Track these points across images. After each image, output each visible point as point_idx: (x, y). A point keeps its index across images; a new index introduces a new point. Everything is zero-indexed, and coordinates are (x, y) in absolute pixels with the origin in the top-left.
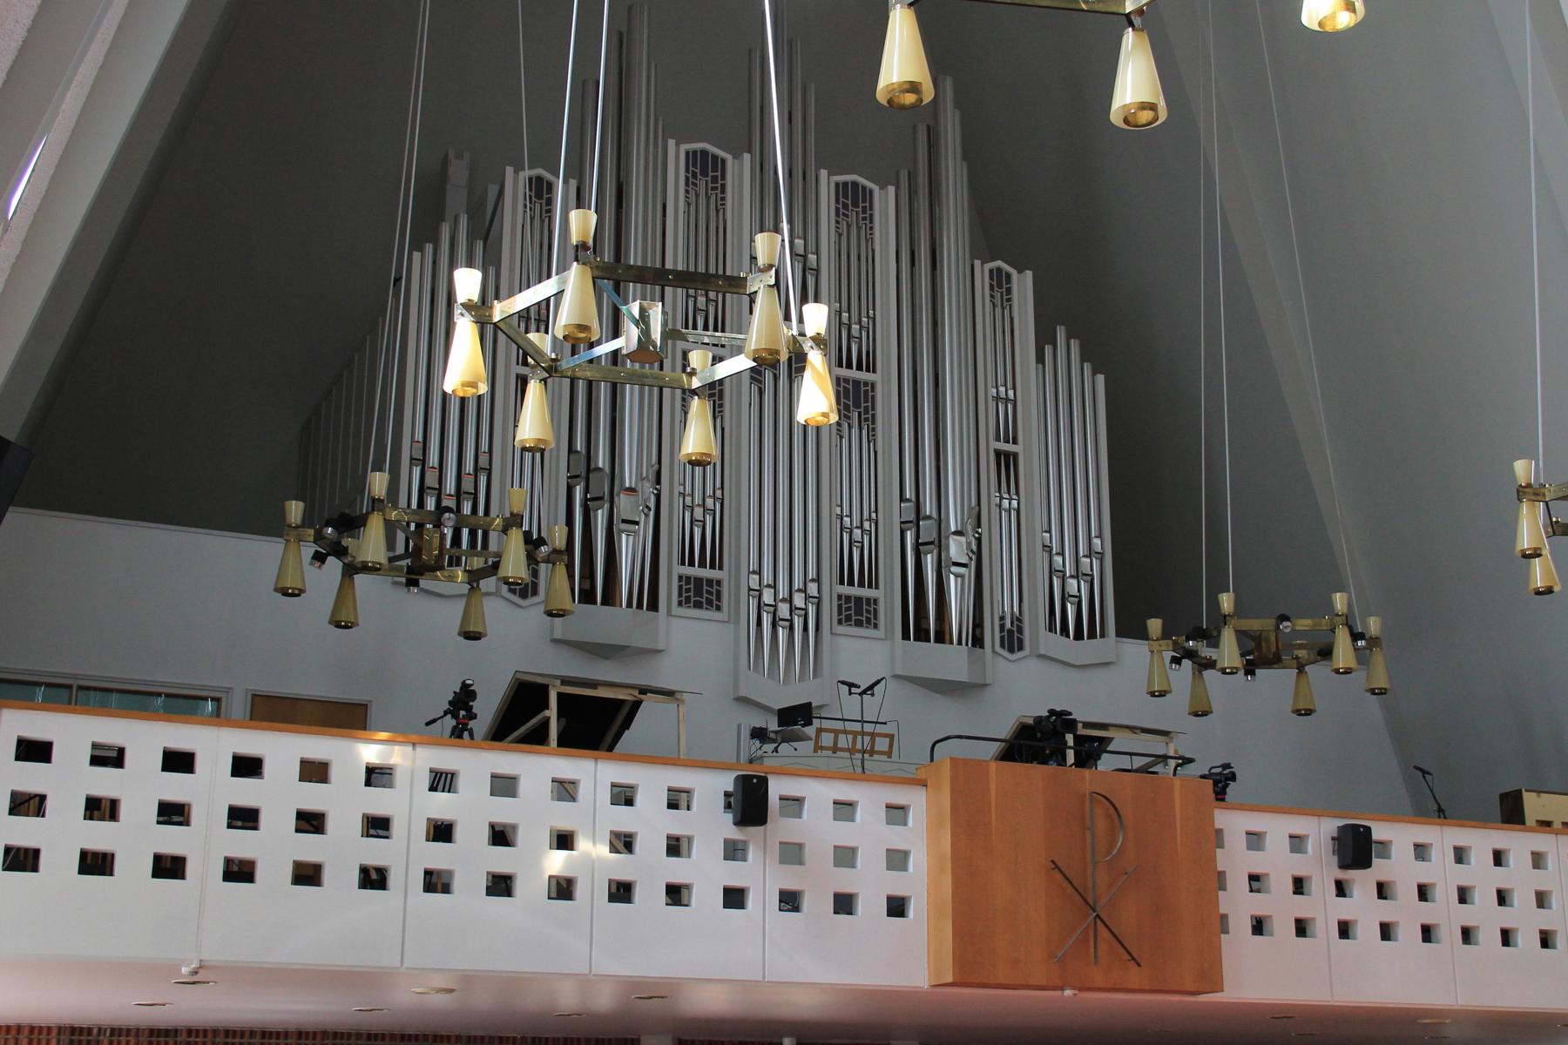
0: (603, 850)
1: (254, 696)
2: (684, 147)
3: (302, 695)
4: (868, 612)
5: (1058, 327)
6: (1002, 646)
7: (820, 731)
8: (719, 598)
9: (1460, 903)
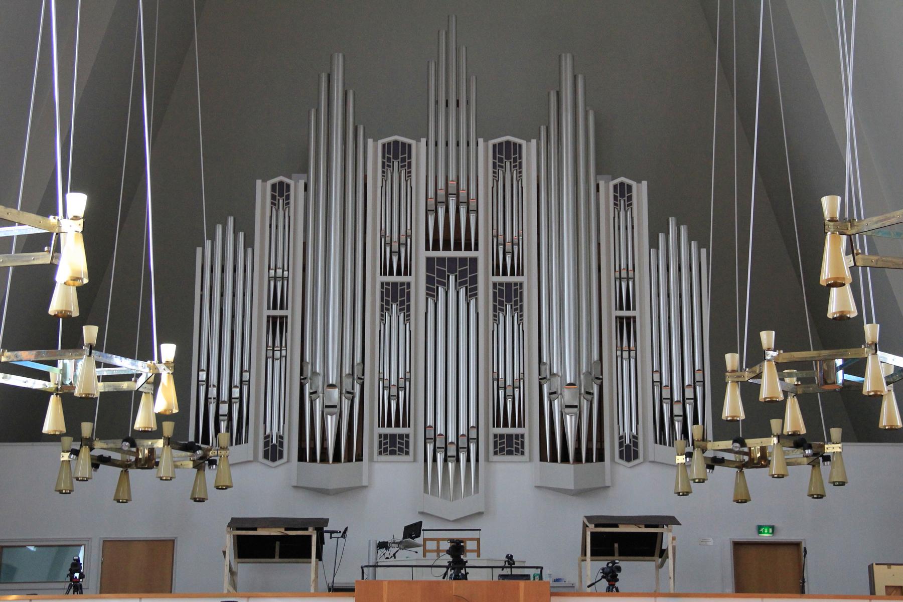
3: (138, 538)
4: (517, 444)
5: (670, 218)
6: (621, 457)
7: (425, 540)
8: (407, 446)
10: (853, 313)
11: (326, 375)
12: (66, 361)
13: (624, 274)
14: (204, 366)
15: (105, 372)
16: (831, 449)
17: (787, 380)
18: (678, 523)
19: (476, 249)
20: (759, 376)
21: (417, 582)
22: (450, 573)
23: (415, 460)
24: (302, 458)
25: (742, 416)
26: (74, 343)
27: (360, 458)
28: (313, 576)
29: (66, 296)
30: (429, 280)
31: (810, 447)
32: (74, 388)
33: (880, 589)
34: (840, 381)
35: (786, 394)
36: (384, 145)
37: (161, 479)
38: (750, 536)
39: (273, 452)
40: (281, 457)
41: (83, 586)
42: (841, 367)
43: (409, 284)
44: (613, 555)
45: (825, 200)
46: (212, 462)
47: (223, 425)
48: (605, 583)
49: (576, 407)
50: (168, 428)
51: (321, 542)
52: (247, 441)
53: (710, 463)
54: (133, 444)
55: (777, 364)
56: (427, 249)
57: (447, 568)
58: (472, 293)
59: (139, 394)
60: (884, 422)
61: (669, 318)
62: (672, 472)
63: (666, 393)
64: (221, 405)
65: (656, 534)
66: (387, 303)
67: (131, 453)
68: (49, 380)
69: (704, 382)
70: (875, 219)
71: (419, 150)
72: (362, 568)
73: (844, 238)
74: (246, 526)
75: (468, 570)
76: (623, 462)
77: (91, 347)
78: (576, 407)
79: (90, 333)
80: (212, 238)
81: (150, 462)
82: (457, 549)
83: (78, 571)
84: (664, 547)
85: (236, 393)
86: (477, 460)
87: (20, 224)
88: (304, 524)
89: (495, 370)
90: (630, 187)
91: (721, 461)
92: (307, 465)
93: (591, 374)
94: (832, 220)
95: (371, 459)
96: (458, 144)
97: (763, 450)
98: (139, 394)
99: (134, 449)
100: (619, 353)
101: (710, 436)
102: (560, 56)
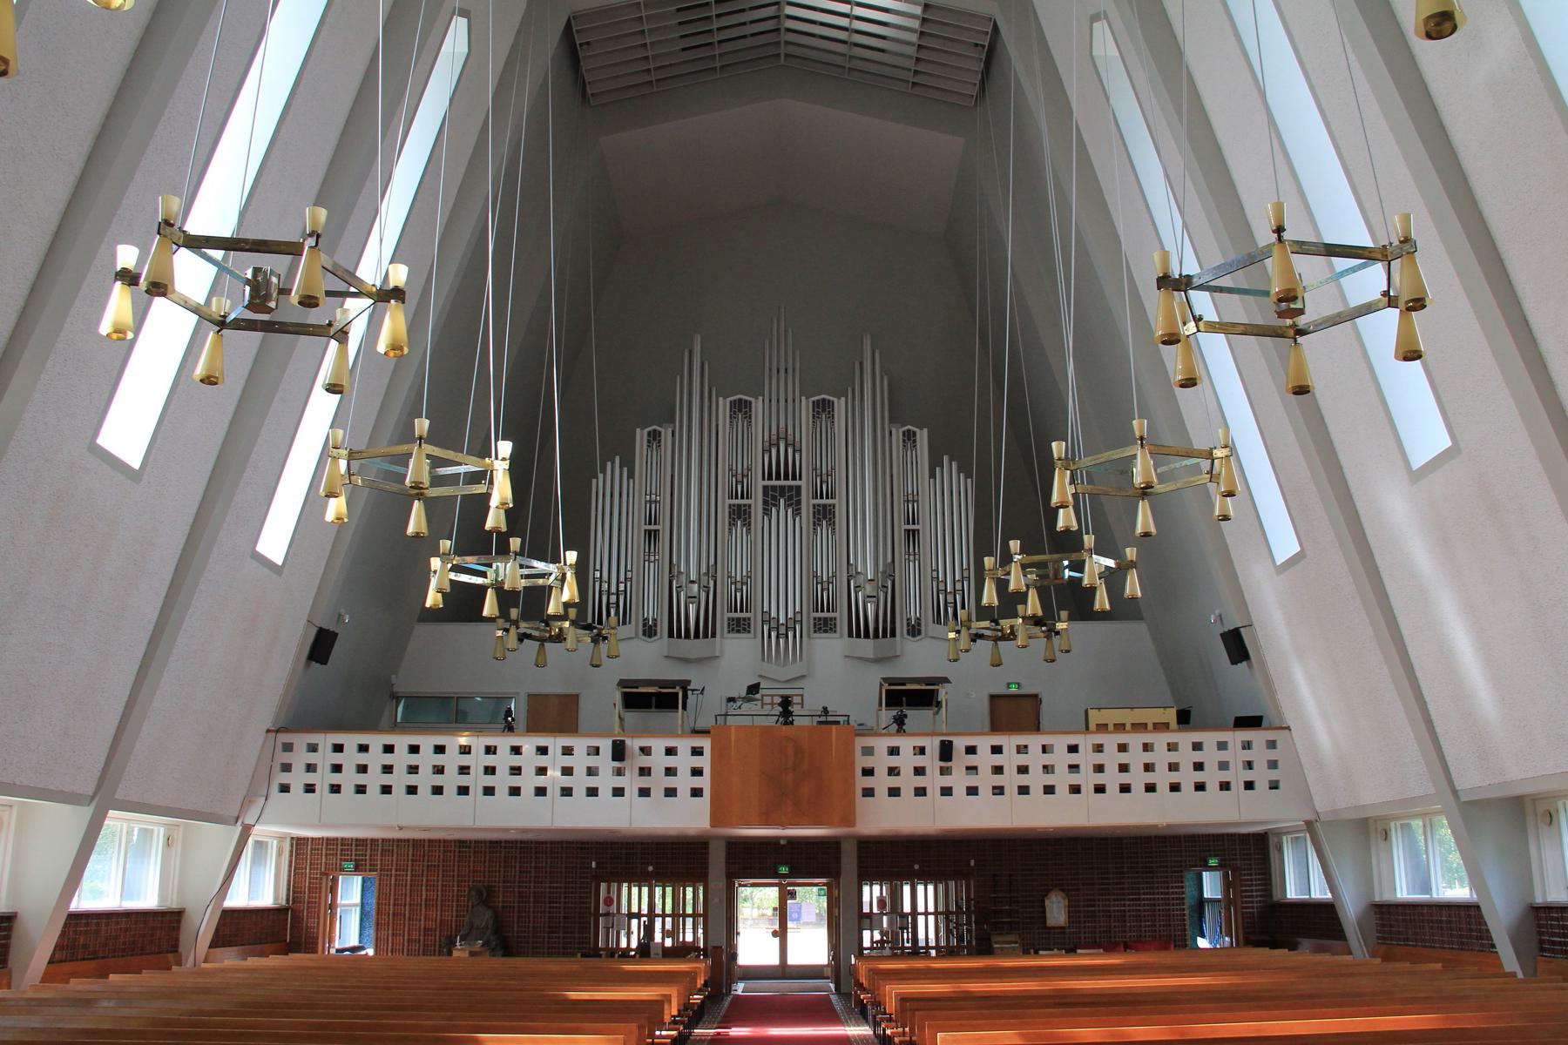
0: (559, 773)
1: (529, 695)
2: (729, 400)
6: (908, 634)
7: (763, 696)
8: (749, 626)
9: (1145, 771)
10: (1075, 526)
11: (688, 574)
12: (499, 564)
13: (910, 498)
14: (598, 567)
15: (526, 571)
16: (1060, 626)
17: (1029, 576)
18: (948, 681)
19: (800, 479)
20: (1009, 574)
21: (756, 727)
22: (781, 719)
23: (755, 637)
24: (671, 635)
25: (996, 603)
26: (504, 551)
27: (714, 635)
28: (680, 722)
29: (497, 517)
30: (765, 502)
31: (1045, 625)
32: (504, 584)
33: (1092, 727)
34: (1067, 577)
35: (1028, 587)
36: (731, 402)
37: (568, 650)
38: (1001, 690)
39: (650, 631)
40: (655, 634)
41: (515, 727)
42: (1067, 567)
43: (750, 506)
44: (902, 706)
45: (1054, 445)
46: (605, 638)
47: (613, 611)
48: (895, 727)
49: (874, 597)
50: (572, 612)
51: (685, 697)
52: (630, 623)
53: (974, 638)
54: (547, 625)
55: (1021, 565)
56: (764, 479)
57: (779, 716)
58: (797, 512)
59: (551, 588)
60: (1097, 606)
61: (944, 530)
62: (947, 644)
63: (942, 587)
64: (611, 596)
65: (933, 690)
66: (735, 413)
67: (547, 631)
68: (486, 578)
69: (969, 578)
70: (1090, 458)
71: (758, 405)
72: (716, 716)
73: (1068, 472)
74: (630, 685)
75: (794, 718)
76: (910, 638)
77: (516, 554)
78: (874, 597)
79: (515, 543)
80: (604, 471)
81: (560, 638)
82: (786, 702)
83: (511, 716)
84: (939, 700)
85: (622, 587)
86: (801, 636)
87: (466, 464)
88: (673, 684)
89: (815, 570)
90: (914, 433)
91: (981, 636)
92: (675, 640)
93: (886, 572)
94: (1059, 459)
95: (722, 637)
96: (794, 401)
97: (1012, 627)
98: (551, 588)
99: (548, 628)
100: (907, 556)
101: (974, 617)
102: (862, 336)
